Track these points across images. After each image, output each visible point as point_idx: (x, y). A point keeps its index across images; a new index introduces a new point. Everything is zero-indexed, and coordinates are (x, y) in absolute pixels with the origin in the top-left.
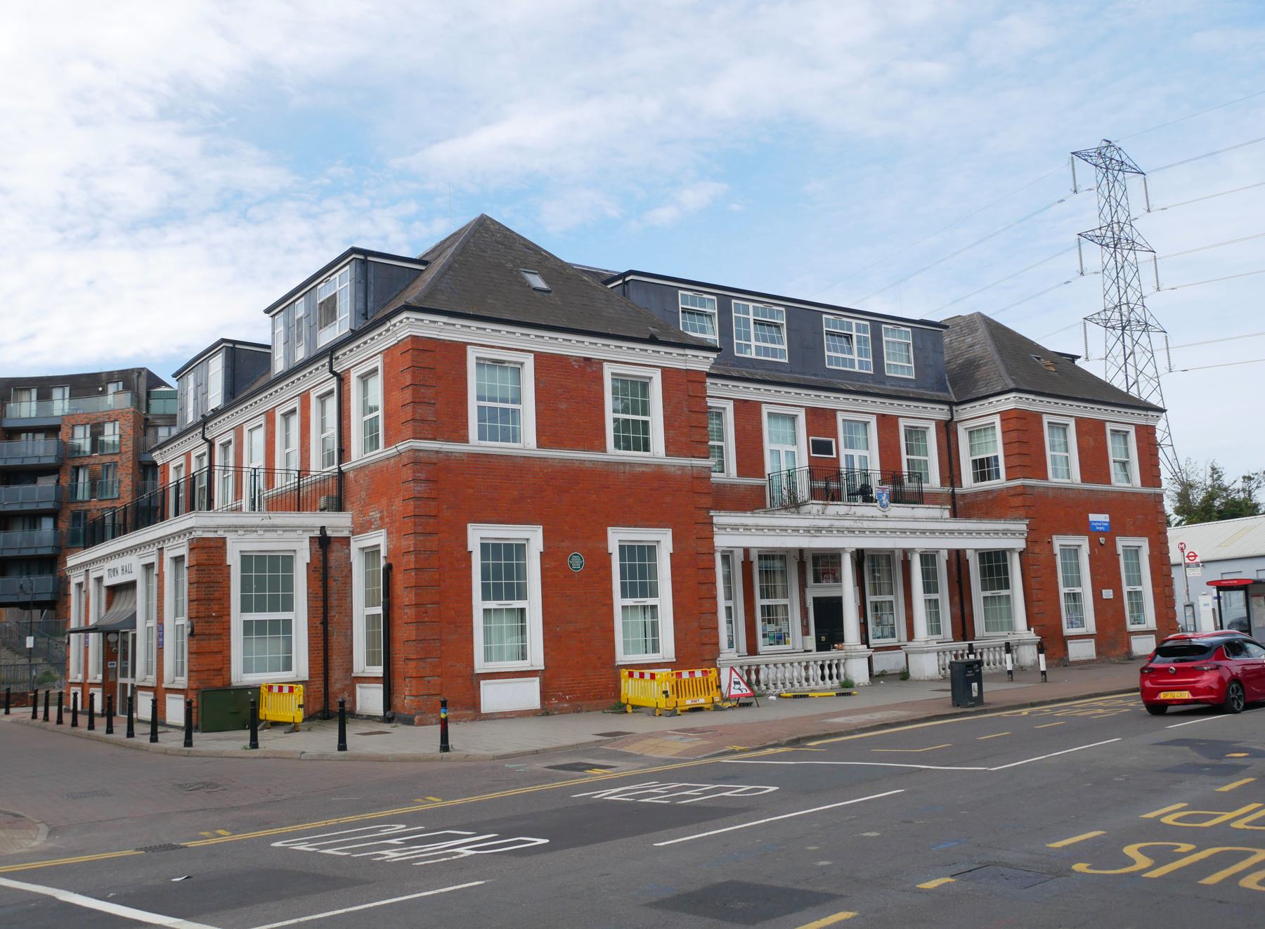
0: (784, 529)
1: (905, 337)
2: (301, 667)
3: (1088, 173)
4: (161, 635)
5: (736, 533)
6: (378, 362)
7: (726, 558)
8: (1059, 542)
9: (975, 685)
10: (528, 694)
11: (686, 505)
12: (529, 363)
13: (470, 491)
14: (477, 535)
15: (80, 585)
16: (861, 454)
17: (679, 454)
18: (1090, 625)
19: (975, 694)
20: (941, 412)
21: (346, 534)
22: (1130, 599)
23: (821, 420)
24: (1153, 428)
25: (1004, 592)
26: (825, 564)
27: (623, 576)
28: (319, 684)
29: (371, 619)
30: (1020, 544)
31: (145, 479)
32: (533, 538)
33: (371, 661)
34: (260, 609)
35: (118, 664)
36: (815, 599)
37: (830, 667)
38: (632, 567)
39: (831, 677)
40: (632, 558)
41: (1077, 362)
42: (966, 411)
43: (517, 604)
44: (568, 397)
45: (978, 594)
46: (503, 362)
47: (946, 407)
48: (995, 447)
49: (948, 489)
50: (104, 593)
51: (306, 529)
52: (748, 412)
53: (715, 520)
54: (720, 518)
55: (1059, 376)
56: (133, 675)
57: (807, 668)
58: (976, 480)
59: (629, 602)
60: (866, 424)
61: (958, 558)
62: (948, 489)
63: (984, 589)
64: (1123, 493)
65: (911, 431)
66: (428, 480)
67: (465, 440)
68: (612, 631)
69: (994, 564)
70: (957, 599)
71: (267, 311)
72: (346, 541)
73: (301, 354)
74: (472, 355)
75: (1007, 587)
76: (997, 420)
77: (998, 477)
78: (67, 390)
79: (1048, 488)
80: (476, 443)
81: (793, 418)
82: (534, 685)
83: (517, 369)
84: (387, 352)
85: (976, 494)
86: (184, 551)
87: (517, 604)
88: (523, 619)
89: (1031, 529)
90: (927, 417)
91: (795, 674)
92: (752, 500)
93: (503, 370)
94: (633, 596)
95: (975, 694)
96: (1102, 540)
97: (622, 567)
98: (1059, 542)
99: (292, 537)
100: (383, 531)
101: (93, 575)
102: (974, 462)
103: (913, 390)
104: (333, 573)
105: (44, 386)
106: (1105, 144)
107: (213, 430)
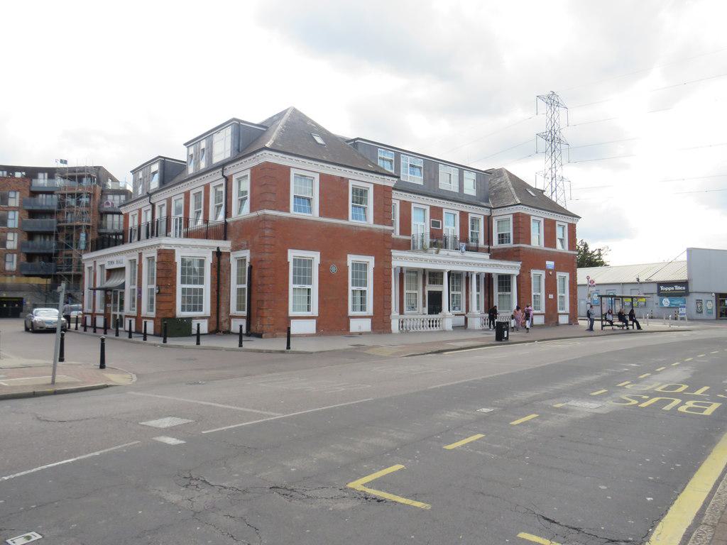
0: (406, 258)
1: (473, 176)
2: (207, 309)
3: (542, 104)
4: (140, 292)
5: (401, 260)
6: (248, 173)
7: (395, 269)
8: (533, 272)
9: (506, 332)
10: (310, 327)
11: (379, 245)
12: (317, 177)
13: (289, 235)
14: (292, 254)
15: (90, 268)
16: (451, 228)
17: (378, 224)
18: (543, 310)
19: (505, 336)
20: (486, 212)
21: (228, 251)
22: (534, 298)
23: (436, 213)
24: (575, 225)
25: (508, 293)
26: (435, 276)
27: (294, 273)
28: (214, 319)
29: (240, 291)
30: (517, 273)
31: (102, 220)
32: (315, 257)
33: (240, 308)
34: (189, 283)
35: (111, 305)
36: (429, 292)
37: (433, 321)
38: (299, 270)
39: (433, 326)
40: (300, 265)
41: (544, 193)
42: (495, 212)
43: (307, 287)
44: (334, 195)
45: (496, 293)
46: (305, 176)
47: (489, 210)
48: (510, 230)
49: (487, 247)
50: (105, 272)
51: (210, 247)
52: (406, 206)
53: (393, 254)
54: (395, 253)
55: (540, 200)
56: (122, 309)
57: (423, 321)
58: (499, 243)
59: (297, 286)
60: (454, 215)
61: (489, 277)
62: (487, 247)
63: (499, 291)
64: (560, 253)
65: (474, 220)
66: (271, 228)
67: (288, 211)
68: (347, 301)
69: (505, 280)
70: (487, 295)
71: (185, 145)
72: (228, 254)
73: (203, 165)
74: (293, 172)
75: (510, 291)
76: (511, 217)
77: (509, 242)
78: (46, 174)
79: (530, 248)
80: (293, 213)
81: (424, 210)
82: (369, 322)
83: (312, 180)
84: (253, 169)
85: (499, 249)
86: (155, 255)
87: (307, 287)
88: (416, 297)
89: (523, 266)
90: (478, 213)
91: (418, 324)
92: (406, 246)
93: (305, 180)
94: (299, 283)
95: (505, 336)
96: (551, 273)
97: (294, 269)
98: (533, 272)
99: (203, 250)
100: (249, 251)
101: (98, 264)
102: (499, 235)
103: (474, 201)
104: (222, 268)
105: (51, 173)
106: (551, 93)
107: (155, 199)
